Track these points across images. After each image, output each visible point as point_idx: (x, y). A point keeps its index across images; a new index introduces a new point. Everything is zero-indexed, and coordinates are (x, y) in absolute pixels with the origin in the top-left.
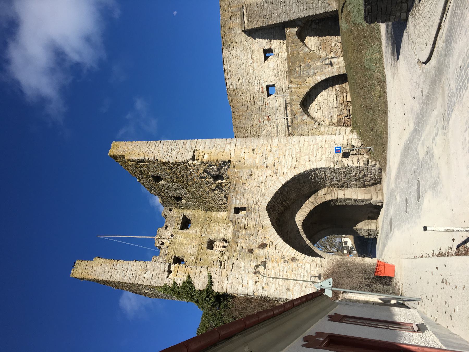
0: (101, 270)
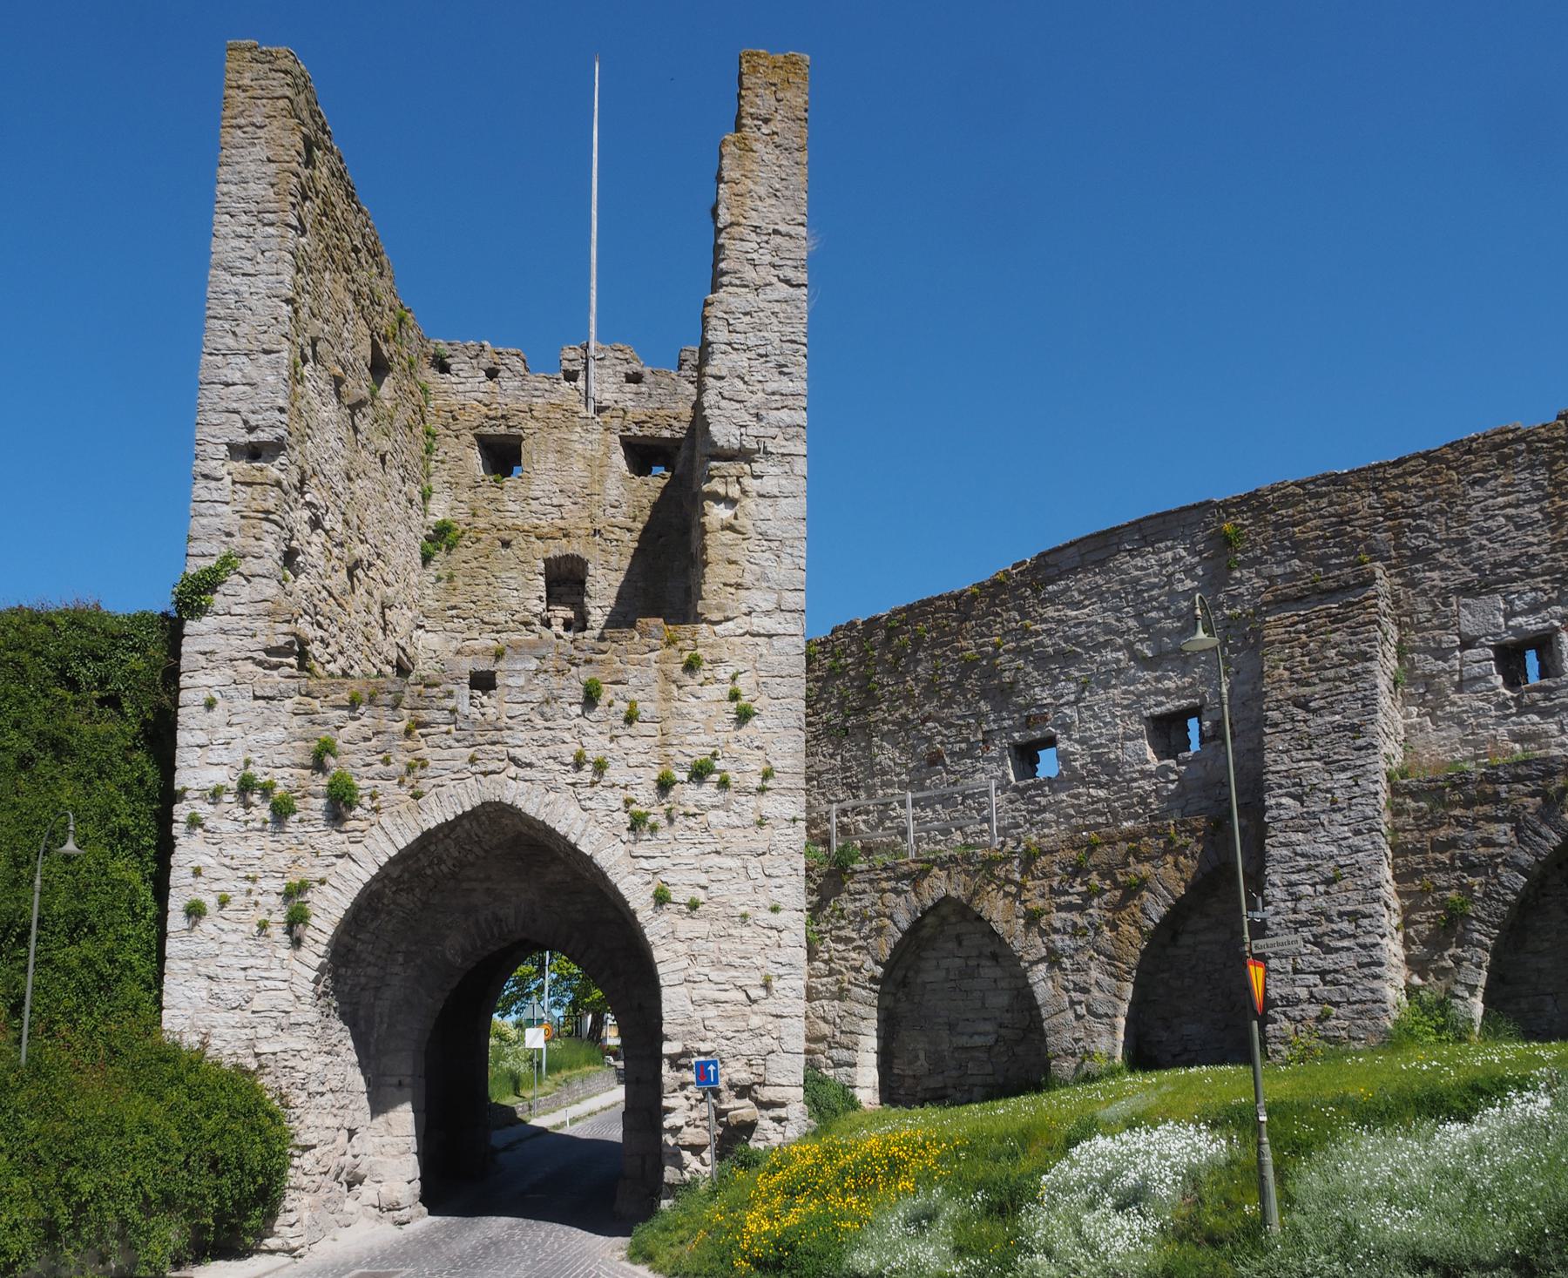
0: (253, 167)
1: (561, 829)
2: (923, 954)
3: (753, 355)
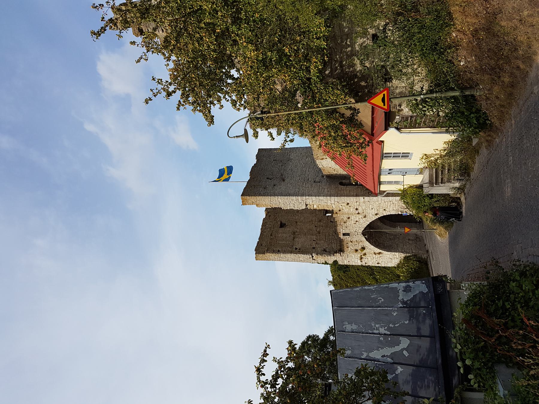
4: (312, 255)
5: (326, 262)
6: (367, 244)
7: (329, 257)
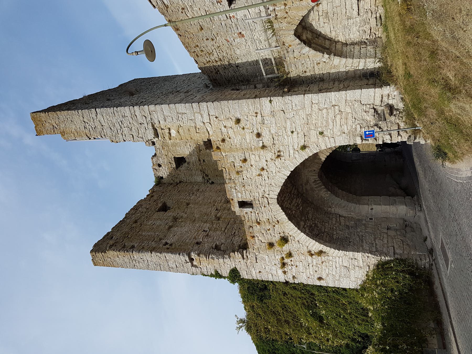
1: (283, 181)
2: (236, 252)
3: (123, 126)
4: (189, 255)
5: (217, 272)
6: (290, 229)
7: (221, 260)
